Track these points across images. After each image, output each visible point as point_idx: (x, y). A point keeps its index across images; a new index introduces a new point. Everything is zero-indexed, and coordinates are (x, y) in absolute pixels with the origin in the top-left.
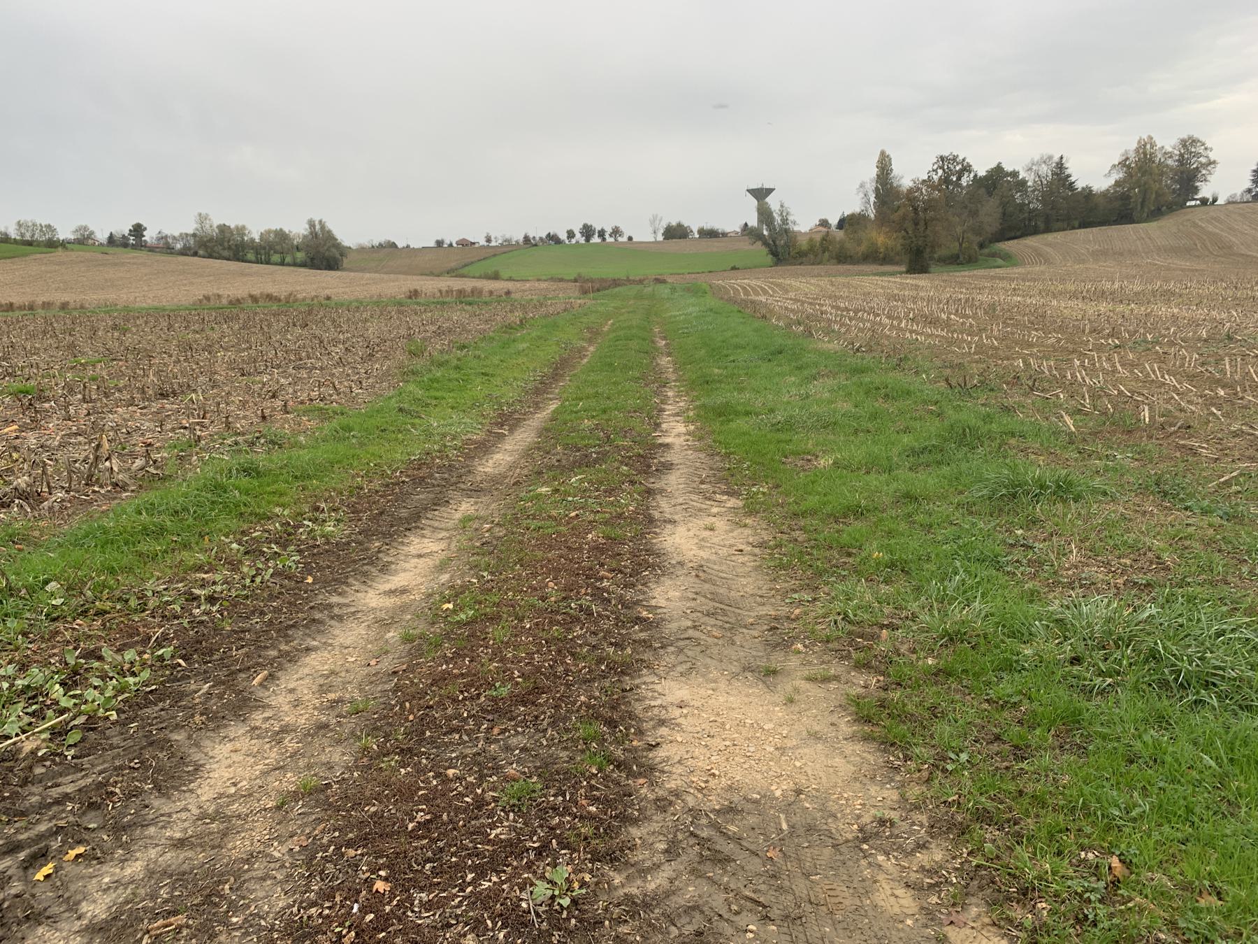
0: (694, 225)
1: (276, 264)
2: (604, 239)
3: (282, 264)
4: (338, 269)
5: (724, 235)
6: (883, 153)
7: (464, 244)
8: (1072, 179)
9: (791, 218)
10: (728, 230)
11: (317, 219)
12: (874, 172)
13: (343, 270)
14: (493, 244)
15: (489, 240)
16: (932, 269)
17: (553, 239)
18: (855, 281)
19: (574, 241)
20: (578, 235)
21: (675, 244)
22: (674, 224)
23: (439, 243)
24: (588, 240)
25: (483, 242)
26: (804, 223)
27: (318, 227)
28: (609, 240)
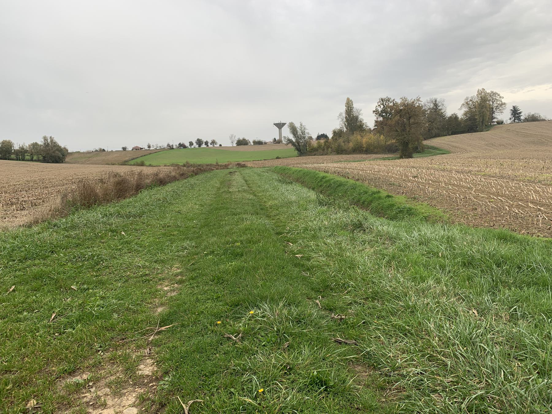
0: (251, 139)
1: (28, 161)
2: (208, 146)
3: (32, 160)
4: (62, 162)
5: (265, 143)
6: (348, 99)
7: (136, 149)
8: (443, 111)
9: (306, 131)
10: (267, 141)
11: (48, 136)
12: (343, 109)
13: (65, 163)
14: (151, 149)
15: (149, 147)
16: (414, 155)
17: (182, 146)
18: (387, 163)
19: (193, 147)
20: (195, 144)
21: (242, 148)
22: (241, 139)
23: (124, 149)
24: (200, 146)
25: (147, 148)
26: (313, 132)
27: (49, 140)
28: (210, 146)
